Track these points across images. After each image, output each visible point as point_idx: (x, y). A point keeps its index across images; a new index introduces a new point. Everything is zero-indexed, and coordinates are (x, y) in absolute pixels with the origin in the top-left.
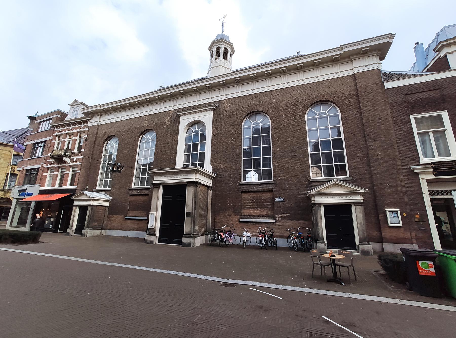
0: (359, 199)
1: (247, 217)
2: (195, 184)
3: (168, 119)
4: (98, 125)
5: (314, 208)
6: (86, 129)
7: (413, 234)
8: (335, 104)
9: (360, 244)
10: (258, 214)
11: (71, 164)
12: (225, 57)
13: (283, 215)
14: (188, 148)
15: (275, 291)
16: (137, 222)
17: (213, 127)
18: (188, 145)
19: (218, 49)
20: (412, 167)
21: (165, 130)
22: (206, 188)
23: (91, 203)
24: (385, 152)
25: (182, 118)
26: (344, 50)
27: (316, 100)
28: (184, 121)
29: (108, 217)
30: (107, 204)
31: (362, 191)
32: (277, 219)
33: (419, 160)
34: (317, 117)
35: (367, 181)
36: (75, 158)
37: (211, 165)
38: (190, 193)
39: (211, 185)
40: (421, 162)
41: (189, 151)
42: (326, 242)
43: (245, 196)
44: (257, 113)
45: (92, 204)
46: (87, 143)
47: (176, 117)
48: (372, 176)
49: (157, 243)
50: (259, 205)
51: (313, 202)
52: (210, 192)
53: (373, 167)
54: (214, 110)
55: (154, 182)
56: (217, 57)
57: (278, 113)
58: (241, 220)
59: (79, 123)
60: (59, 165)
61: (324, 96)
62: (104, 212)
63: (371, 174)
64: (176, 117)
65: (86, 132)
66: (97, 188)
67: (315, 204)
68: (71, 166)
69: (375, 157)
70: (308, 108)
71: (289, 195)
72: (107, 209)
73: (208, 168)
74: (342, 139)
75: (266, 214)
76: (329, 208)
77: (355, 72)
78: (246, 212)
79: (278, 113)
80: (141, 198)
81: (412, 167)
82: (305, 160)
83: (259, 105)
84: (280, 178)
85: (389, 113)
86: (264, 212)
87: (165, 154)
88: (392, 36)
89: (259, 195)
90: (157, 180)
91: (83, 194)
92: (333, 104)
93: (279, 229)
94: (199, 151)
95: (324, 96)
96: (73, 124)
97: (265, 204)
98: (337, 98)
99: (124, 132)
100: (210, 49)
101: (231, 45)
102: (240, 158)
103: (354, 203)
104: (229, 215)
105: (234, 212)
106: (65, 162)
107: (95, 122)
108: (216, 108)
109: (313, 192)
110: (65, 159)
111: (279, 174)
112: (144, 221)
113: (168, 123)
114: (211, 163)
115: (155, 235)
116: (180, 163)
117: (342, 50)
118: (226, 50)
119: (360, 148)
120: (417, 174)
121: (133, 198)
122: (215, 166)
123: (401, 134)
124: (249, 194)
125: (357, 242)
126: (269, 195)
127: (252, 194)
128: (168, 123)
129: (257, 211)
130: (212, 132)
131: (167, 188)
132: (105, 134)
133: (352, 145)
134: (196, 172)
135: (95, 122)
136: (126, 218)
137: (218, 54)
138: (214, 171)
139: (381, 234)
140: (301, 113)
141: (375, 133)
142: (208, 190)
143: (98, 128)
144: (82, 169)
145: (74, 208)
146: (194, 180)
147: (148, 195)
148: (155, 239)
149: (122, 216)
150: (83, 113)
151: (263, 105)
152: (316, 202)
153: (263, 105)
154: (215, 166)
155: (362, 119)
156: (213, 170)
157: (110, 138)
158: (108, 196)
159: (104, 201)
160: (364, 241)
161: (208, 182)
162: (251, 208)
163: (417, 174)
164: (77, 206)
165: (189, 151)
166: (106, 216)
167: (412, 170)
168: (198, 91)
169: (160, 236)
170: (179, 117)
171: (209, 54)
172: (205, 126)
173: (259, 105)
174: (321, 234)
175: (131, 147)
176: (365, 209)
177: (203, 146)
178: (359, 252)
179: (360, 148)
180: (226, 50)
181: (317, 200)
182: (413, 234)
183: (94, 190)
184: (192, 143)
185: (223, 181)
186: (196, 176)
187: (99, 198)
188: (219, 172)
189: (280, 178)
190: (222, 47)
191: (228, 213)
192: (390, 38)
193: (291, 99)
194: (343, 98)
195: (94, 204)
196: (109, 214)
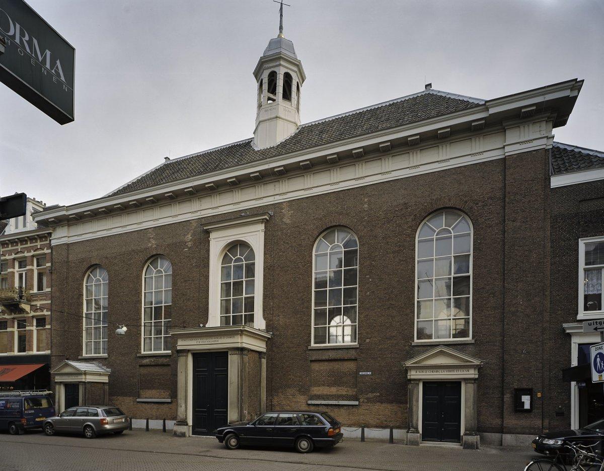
0: (472, 374)
1: (318, 397)
2: (241, 350)
3: (189, 237)
4: (68, 245)
5: (410, 386)
6: (46, 251)
7: (546, 422)
8: (467, 214)
9: (466, 434)
10: (334, 393)
11: (33, 314)
12: (287, 96)
13: (370, 395)
14: (226, 287)
15: (222, 416)
16: (155, 406)
17: (265, 254)
18: (226, 283)
19: (273, 76)
20: (565, 325)
21: (185, 253)
22: (257, 355)
23: (83, 378)
24: (530, 300)
25: (213, 236)
26: (492, 111)
27: (435, 207)
28: (218, 243)
29: (110, 400)
30: (105, 379)
31: (476, 362)
32: (361, 400)
33: (577, 314)
34: (435, 237)
35: (496, 346)
36: (38, 303)
37: (265, 318)
38: (233, 361)
39: (264, 350)
40: (579, 317)
41: (227, 311)
42: (421, 432)
43: (316, 367)
44: (339, 228)
45: (83, 380)
46: (54, 277)
47: (203, 230)
48: (504, 337)
49: (191, 435)
50: (337, 380)
51: (409, 377)
52: (264, 361)
53: (507, 324)
54: (266, 222)
55: (179, 348)
56: (271, 96)
57: (372, 230)
58: (310, 402)
59: (32, 239)
60: (13, 316)
61: (450, 200)
62: (102, 392)
63: (503, 335)
64: (203, 230)
65: (48, 257)
66: (84, 355)
67: (410, 380)
68: (33, 317)
69: (513, 309)
70: (422, 221)
71: (380, 366)
72: (107, 387)
73: (260, 323)
74: (469, 277)
75: (345, 393)
76: (429, 385)
77: (506, 154)
78: (316, 390)
79: (372, 230)
80: (157, 369)
81: (565, 325)
82: (408, 311)
83: (341, 214)
84: (368, 341)
85: (548, 233)
86: (343, 391)
87: (189, 300)
88: (576, 85)
89: (336, 366)
90: (182, 344)
91: (67, 365)
92: (464, 215)
93: (363, 414)
94: (244, 295)
95: (450, 200)
96: (22, 241)
97: (345, 379)
98: (471, 204)
99: (115, 257)
100: (257, 74)
101: (298, 65)
102: (309, 308)
103: (465, 380)
104: (293, 395)
105: (299, 391)
106: (22, 311)
107: (61, 237)
108: (268, 217)
109: (409, 363)
110: (23, 306)
111: (367, 333)
112: (166, 406)
113: (189, 244)
114: (264, 315)
115: (187, 425)
116: (215, 320)
117: (487, 109)
118: (288, 77)
119: (493, 294)
120: (569, 336)
121: (144, 371)
122: (270, 321)
123: (559, 271)
124: (322, 364)
125: (462, 434)
126: (351, 366)
127: (326, 363)
128: (189, 244)
129: (333, 390)
130: (265, 263)
131: (198, 357)
132: (82, 261)
133: (483, 288)
134: (241, 333)
135: (61, 237)
136: (138, 400)
137: (272, 89)
138: (269, 327)
139: (503, 422)
140: (409, 232)
141: (520, 268)
142: (260, 358)
143: (68, 250)
144: (54, 323)
145: (57, 387)
146: (239, 345)
147: (169, 365)
148: (187, 430)
149: (131, 398)
150: (37, 222)
151: (347, 214)
152: (412, 377)
153: (347, 214)
154: (270, 321)
155: (504, 244)
156: (267, 326)
157: (93, 267)
158: (104, 367)
159: (100, 375)
160: (469, 432)
161: (261, 346)
162: (324, 385)
163: (569, 336)
164: (61, 383)
165: (228, 294)
166: (107, 397)
167: (564, 330)
168: (237, 184)
169: (193, 426)
170: (208, 232)
171: (256, 85)
172: (252, 250)
173: (341, 214)
174: (414, 421)
175: (131, 286)
176: (479, 387)
177: (251, 284)
178: (461, 445)
179: (493, 294)
180: (288, 77)
181: (413, 375)
182: (546, 422)
183: (80, 357)
184: (232, 281)
185: (283, 344)
186: (242, 338)
187: (90, 371)
188: (278, 330)
189: (368, 341)
190: (281, 73)
191: (290, 391)
192: (572, 89)
193: (395, 204)
194: (480, 204)
195: (87, 380)
196: (111, 394)
